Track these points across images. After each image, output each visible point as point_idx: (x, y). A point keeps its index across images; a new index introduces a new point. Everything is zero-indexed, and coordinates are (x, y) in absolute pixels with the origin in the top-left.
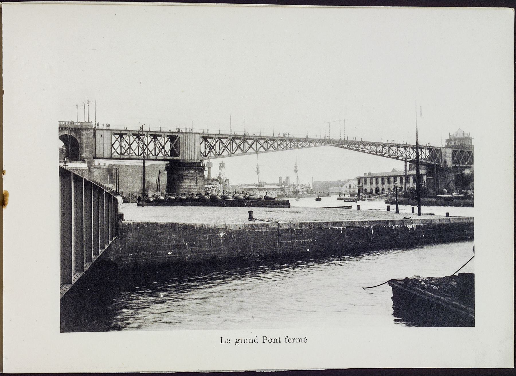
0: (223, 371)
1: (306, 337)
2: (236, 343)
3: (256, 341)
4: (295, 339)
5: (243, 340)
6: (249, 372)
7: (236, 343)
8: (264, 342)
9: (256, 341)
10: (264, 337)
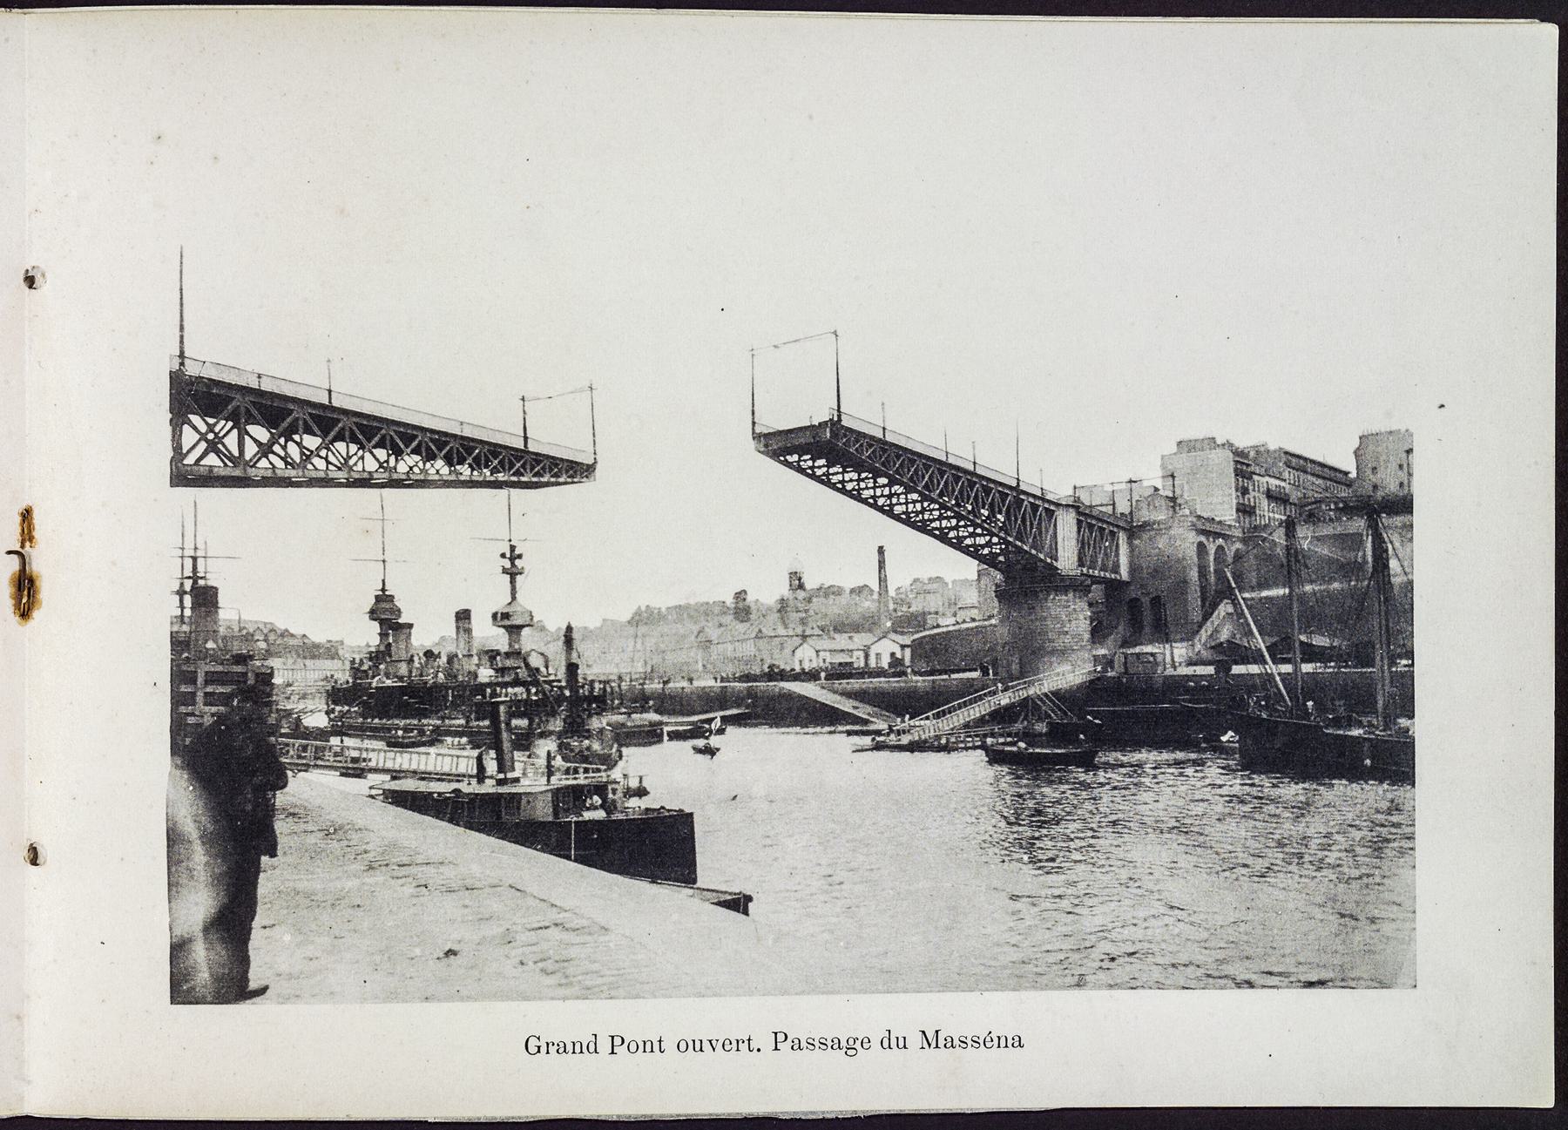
0: (678, 1115)
1: (990, 1033)
2: (848, 1049)
3: (592, 1048)
4: (743, 1042)
5: (553, 1044)
6: (757, 1118)
7: (848, 1049)
8: (613, 1053)
9: (592, 1048)
10: (776, 1033)
